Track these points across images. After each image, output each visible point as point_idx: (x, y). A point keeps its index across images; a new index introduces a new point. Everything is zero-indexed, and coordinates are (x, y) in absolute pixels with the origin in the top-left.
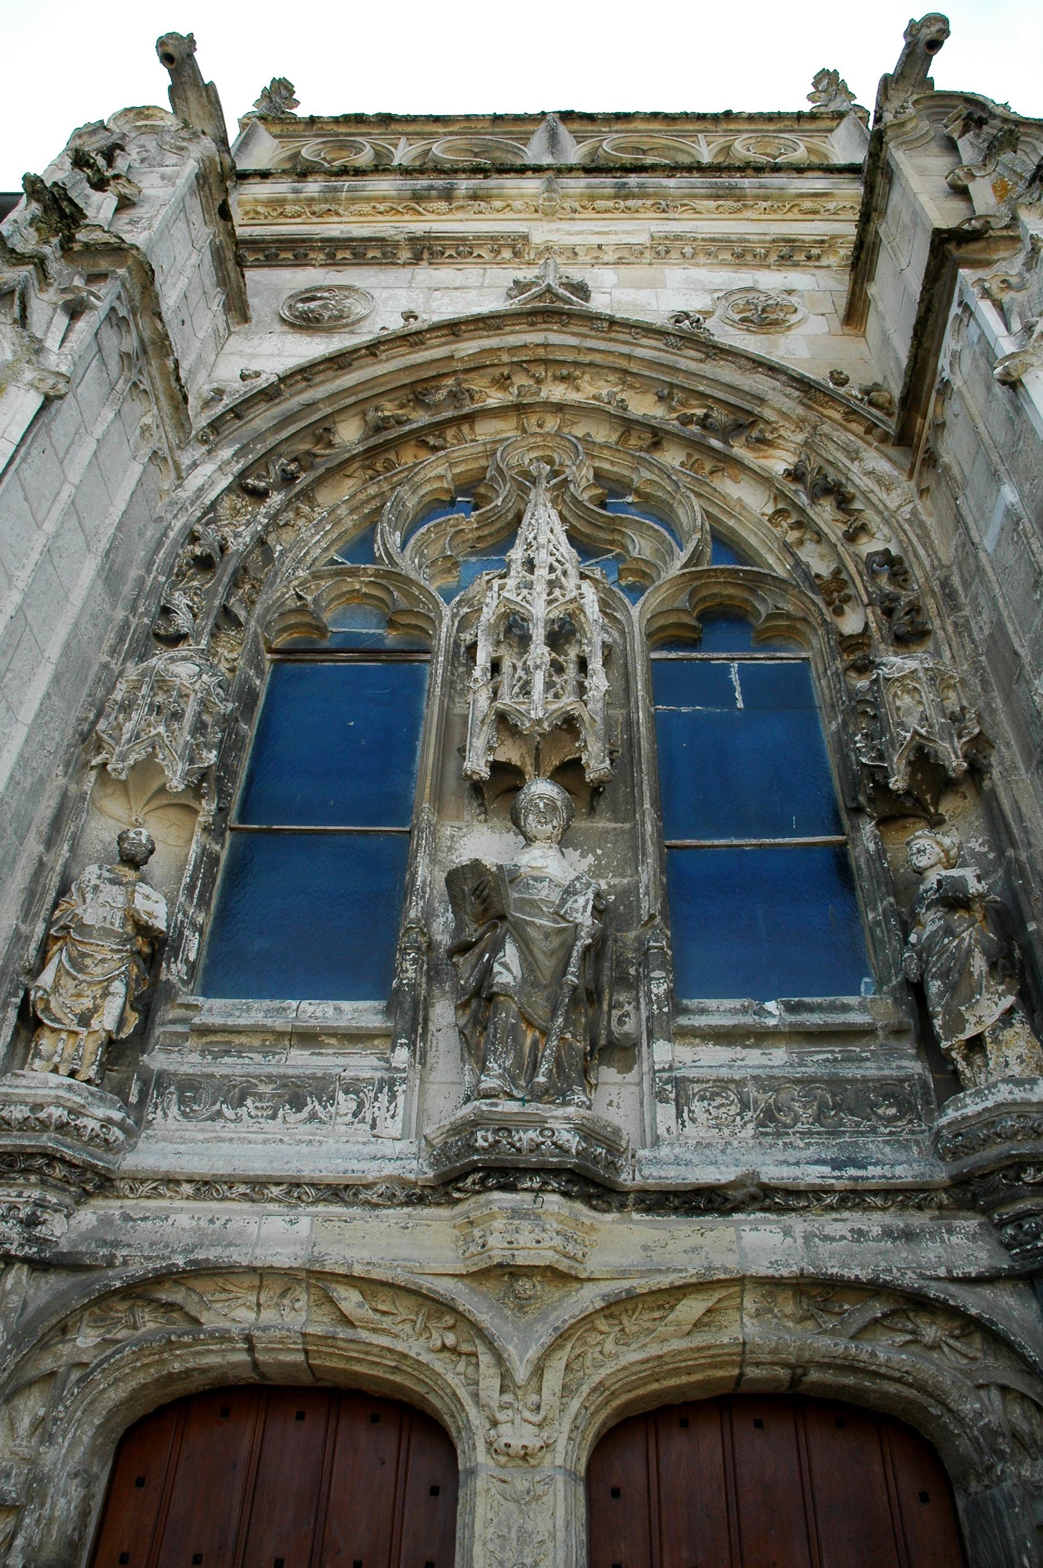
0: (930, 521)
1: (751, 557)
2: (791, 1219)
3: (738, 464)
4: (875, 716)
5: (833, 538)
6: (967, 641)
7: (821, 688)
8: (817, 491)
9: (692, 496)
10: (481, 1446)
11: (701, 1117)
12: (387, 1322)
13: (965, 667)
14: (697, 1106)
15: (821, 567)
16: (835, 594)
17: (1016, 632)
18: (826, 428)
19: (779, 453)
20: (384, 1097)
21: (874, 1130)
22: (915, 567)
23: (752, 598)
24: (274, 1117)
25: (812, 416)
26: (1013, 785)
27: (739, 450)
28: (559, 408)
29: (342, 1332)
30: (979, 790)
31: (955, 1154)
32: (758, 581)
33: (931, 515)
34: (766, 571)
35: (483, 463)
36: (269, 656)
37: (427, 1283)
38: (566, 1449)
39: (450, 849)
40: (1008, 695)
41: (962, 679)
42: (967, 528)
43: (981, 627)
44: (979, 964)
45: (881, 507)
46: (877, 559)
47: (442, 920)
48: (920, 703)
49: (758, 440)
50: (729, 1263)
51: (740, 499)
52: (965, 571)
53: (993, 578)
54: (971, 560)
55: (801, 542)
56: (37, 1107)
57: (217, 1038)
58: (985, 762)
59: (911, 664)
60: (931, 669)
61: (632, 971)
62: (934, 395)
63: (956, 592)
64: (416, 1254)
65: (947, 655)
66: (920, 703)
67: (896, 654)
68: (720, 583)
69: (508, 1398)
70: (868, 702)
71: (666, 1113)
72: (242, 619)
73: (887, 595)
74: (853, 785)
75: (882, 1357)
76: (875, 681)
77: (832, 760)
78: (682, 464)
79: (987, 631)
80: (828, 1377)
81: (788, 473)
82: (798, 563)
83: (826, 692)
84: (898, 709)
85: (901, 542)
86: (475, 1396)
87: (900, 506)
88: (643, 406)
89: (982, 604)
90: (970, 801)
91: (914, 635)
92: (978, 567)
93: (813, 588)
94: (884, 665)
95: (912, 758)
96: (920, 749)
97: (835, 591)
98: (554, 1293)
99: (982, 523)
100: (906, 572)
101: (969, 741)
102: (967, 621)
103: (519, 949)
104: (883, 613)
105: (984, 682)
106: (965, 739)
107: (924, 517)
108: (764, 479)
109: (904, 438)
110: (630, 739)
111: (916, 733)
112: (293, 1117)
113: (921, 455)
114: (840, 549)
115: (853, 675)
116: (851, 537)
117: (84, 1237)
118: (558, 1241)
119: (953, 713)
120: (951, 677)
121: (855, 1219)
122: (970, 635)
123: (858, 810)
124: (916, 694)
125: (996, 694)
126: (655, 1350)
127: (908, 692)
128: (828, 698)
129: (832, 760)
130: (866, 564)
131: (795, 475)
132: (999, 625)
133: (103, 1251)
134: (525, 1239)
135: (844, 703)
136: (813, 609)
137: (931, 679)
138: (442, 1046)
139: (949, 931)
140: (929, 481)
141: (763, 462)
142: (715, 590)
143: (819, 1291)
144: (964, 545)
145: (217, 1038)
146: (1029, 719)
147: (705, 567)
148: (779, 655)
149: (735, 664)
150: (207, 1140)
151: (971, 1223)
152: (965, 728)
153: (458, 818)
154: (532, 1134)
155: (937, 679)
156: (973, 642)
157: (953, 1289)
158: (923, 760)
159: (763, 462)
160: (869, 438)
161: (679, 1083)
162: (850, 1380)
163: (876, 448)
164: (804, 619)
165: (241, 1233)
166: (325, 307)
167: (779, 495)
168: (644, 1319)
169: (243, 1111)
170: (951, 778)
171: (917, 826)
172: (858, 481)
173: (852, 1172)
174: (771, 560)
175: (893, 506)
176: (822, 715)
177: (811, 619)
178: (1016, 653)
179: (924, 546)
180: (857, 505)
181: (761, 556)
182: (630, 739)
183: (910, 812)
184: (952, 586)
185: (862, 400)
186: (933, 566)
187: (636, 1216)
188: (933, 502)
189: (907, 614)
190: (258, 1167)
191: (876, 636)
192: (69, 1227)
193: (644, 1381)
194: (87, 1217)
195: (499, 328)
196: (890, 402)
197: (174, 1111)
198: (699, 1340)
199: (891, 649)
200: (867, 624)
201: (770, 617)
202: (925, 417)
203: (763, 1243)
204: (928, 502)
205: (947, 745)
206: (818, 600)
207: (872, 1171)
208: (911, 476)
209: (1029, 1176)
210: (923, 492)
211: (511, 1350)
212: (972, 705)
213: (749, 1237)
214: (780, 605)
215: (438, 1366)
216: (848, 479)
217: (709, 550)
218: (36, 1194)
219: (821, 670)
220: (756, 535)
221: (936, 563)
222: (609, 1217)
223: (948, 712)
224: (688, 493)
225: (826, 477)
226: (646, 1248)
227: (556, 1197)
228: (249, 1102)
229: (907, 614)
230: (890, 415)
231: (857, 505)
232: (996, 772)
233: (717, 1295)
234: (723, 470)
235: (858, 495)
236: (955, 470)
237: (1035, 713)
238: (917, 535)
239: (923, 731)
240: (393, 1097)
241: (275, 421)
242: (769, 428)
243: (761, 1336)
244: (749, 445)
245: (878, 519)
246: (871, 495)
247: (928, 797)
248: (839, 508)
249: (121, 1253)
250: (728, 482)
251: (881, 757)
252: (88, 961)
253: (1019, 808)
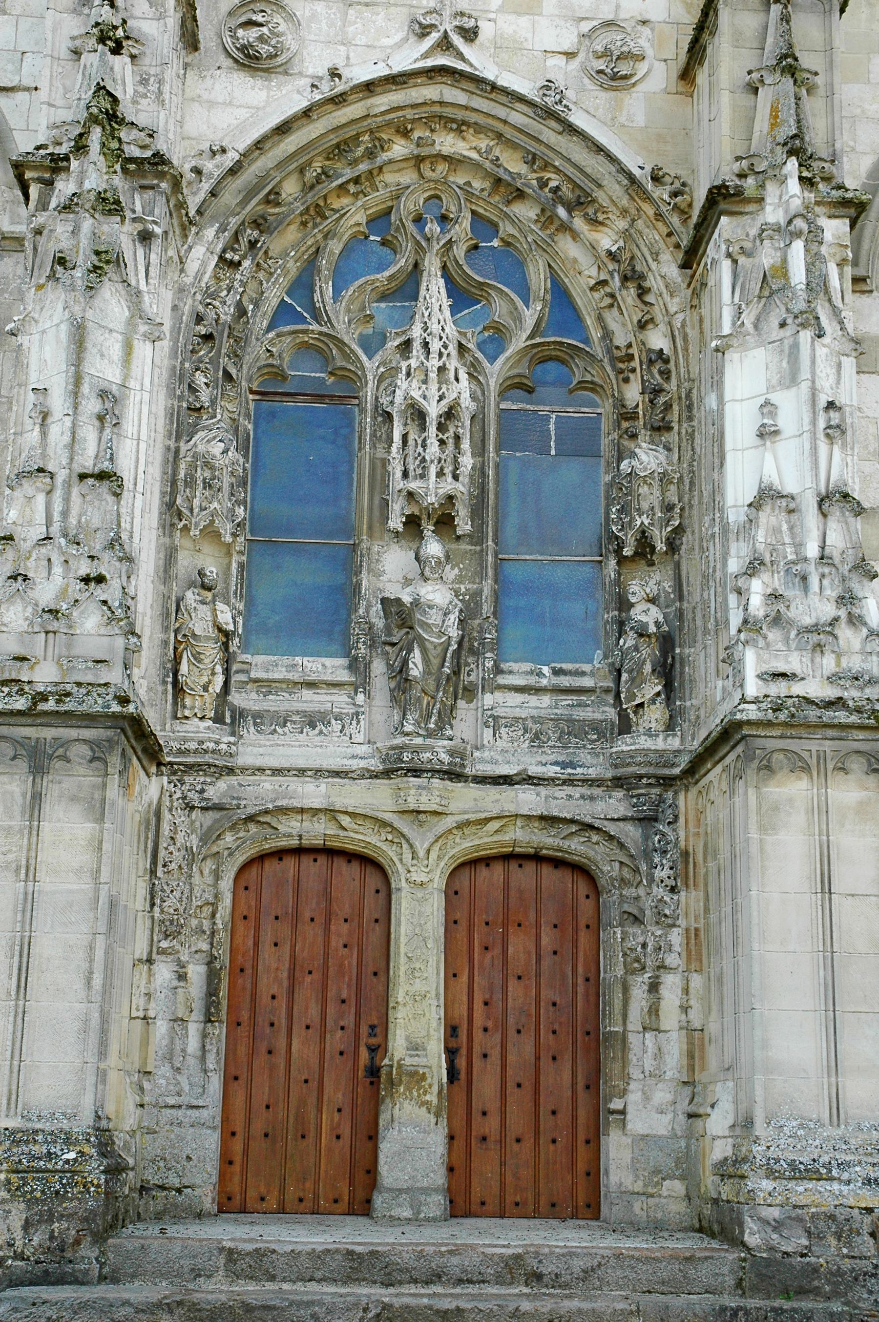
2: (540, 789)
10: (403, 880)
11: (505, 736)
12: (361, 829)
14: (503, 730)
19: (606, 229)
20: (354, 722)
21: (584, 746)
24: (302, 732)
27: (579, 223)
28: (450, 160)
29: (342, 833)
31: (616, 766)
35: (390, 204)
36: (251, 397)
37: (380, 815)
38: (439, 881)
39: (378, 561)
44: (648, 668)
47: (374, 609)
50: (511, 808)
56: (201, 742)
57: (266, 686)
61: (476, 644)
64: (375, 802)
69: (415, 862)
71: (488, 733)
72: (235, 376)
75: (573, 847)
80: (551, 853)
86: (401, 860)
87: (676, 313)
88: (513, 164)
98: (436, 819)
103: (421, 651)
110: (483, 483)
112: (312, 733)
117: (224, 795)
118: (438, 799)
121: (569, 790)
126: (477, 842)
133: (235, 802)
134: (424, 799)
138: (378, 685)
139: (636, 649)
143: (549, 820)
145: (266, 686)
148: (583, 410)
150: (271, 746)
151: (619, 794)
153: (381, 539)
154: (428, 755)
157: (606, 823)
161: (495, 718)
162: (560, 854)
165: (295, 791)
166: (261, 39)
168: (473, 829)
169: (286, 729)
173: (570, 771)
182: (483, 483)
187: (472, 785)
190: (301, 763)
192: (218, 789)
193: (471, 853)
194: (222, 785)
195: (405, 83)
197: (252, 729)
198: (496, 838)
203: (528, 800)
205: (658, 533)
207: (579, 770)
209: (644, 781)
211: (417, 844)
213: (521, 796)
215: (384, 848)
218: (202, 779)
222: (460, 785)
226: (475, 800)
227: (437, 780)
228: (288, 724)
233: (505, 820)
240: (358, 722)
241: (240, 197)
243: (522, 837)
249: (243, 802)
252: (202, 657)
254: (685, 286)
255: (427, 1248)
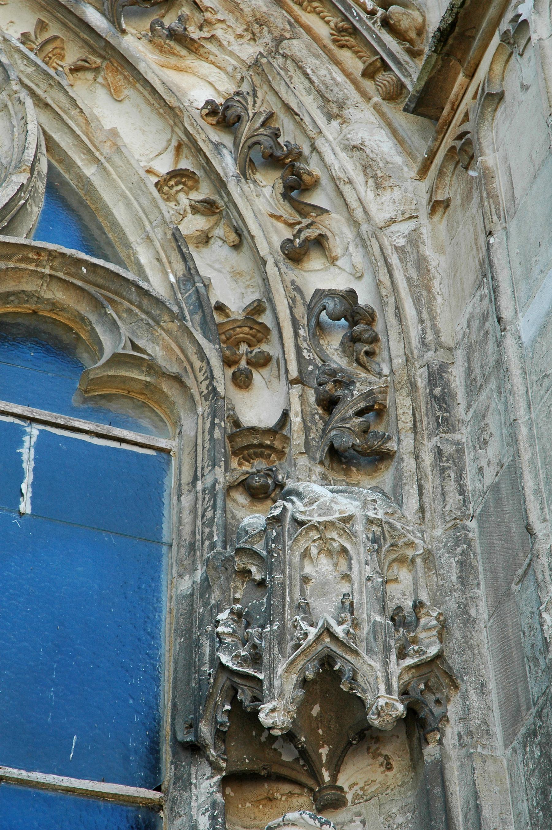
0: (436, 260)
1: (109, 243)
3: (126, 65)
4: (261, 584)
5: (263, 249)
6: (451, 486)
7: (179, 512)
8: (256, 155)
9: (29, 102)
13: (438, 532)
15: (232, 293)
16: (244, 348)
17: (537, 492)
18: (297, 47)
19: (204, 68)
22: (393, 334)
23: (92, 318)
25: (279, 18)
26: (478, 764)
27: (134, 43)
30: (416, 760)
32: (116, 289)
33: (441, 250)
34: (130, 276)
40: (501, 599)
41: (428, 552)
42: (495, 290)
43: (481, 470)
45: (359, 214)
46: (330, 304)
48: (346, 577)
49: (172, 35)
51: (114, 133)
52: (476, 365)
53: (520, 389)
54: (491, 347)
55: (205, 239)
58: (437, 711)
59: (346, 505)
60: (380, 523)
62: (496, 40)
63: (453, 396)
65: (412, 503)
66: (346, 577)
67: (324, 480)
68: (42, 276)
70: (255, 554)
73: (333, 373)
74: (197, 701)
76: (277, 520)
77: (169, 647)
78: (25, 38)
79: (489, 479)
81: (212, 110)
82: (191, 274)
83: (187, 518)
84: (305, 579)
85: (378, 284)
87: (393, 221)
89: (492, 428)
90: (395, 776)
91: (363, 454)
92: (499, 363)
93: (206, 325)
94: (299, 495)
95: (310, 675)
96: (327, 661)
97: (244, 343)
99: (523, 287)
100: (375, 339)
101: (416, 666)
102: (460, 452)
104: (319, 402)
105: (464, 565)
106: (409, 661)
107: (428, 251)
108: (166, 108)
109: (428, 103)
111: (327, 630)
113: (449, 141)
114: (271, 268)
115: (241, 498)
116: (294, 254)
119: (399, 608)
120: (410, 544)
122: (460, 477)
123: (195, 749)
124: (343, 563)
125: (481, 592)
127: (330, 553)
128: (187, 530)
129: (169, 647)
130: (309, 307)
131: (223, 116)
132: (512, 472)
135: (213, 546)
136: (198, 364)
137: (375, 540)
140: (452, 189)
141: (172, 76)
142: (29, 286)
144: (485, 318)
146: (528, 650)
147: (21, 240)
149: (35, 430)
152: (415, 641)
155: (384, 540)
156: (462, 492)
158: (328, 683)
159: (172, 76)
160: (368, 85)
163: (376, 107)
164: (177, 379)
167: (187, 144)
170: (370, 727)
171: (296, 801)
172: (329, 157)
174: (144, 257)
175: (380, 215)
176: (170, 560)
177: (190, 382)
178: (529, 530)
179: (417, 301)
180: (318, 199)
181: (128, 246)
183: (284, 771)
184: (446, 385)
185: (372, 13)
186: (423, 343)
188: (451, 229)
189: (360, 413)
191: (298, 439)
196: (420, 32)
199: (319, 469)
200: (285, 415)
201: (118, 359)
202: (471, 76)
204: (442, 226)
205: (378, 665)
206: (211, 351)
208: (423, 171)
210: (437, 206)
212: (435, 603)
214: (140, 343)
216: (314, 148)
217: (35, 211)
219: (186, 478)
220: (128, 205)
221: (430, 337)
223: (391, 605)
224: (24, 95)
225: (276, 134)
229: (360, 413)
230: (414, 54)
231: (318, 199)
232: (452, 731)
234: (97, 70)
235: (324, 180)
236: (500, 183)
237: (539, 643)
238: (409, 280)
239: (339, 631)
242: (198, 17)
244: (153, 37)
245: (348, 233)
246: (346, 189)
247: (324, 751)
248: (285, 196)
250: (101, 94)
251: (256, 659)
253: (478, 809)
254: (413, 173)
255: (314, 161)
